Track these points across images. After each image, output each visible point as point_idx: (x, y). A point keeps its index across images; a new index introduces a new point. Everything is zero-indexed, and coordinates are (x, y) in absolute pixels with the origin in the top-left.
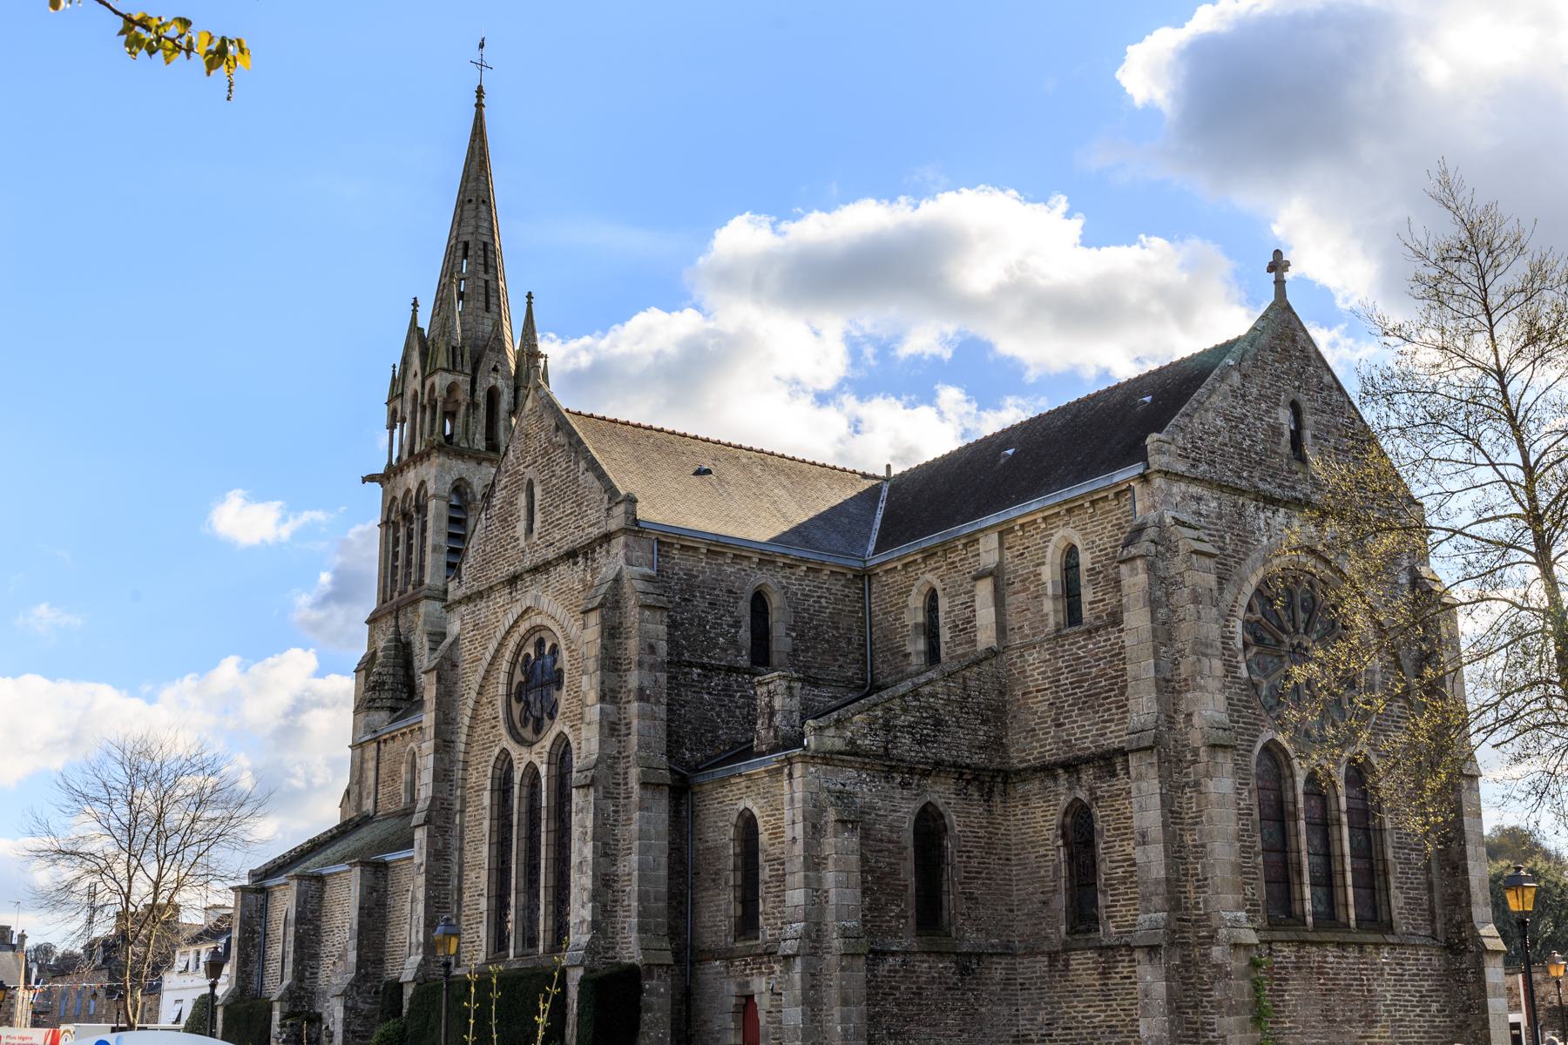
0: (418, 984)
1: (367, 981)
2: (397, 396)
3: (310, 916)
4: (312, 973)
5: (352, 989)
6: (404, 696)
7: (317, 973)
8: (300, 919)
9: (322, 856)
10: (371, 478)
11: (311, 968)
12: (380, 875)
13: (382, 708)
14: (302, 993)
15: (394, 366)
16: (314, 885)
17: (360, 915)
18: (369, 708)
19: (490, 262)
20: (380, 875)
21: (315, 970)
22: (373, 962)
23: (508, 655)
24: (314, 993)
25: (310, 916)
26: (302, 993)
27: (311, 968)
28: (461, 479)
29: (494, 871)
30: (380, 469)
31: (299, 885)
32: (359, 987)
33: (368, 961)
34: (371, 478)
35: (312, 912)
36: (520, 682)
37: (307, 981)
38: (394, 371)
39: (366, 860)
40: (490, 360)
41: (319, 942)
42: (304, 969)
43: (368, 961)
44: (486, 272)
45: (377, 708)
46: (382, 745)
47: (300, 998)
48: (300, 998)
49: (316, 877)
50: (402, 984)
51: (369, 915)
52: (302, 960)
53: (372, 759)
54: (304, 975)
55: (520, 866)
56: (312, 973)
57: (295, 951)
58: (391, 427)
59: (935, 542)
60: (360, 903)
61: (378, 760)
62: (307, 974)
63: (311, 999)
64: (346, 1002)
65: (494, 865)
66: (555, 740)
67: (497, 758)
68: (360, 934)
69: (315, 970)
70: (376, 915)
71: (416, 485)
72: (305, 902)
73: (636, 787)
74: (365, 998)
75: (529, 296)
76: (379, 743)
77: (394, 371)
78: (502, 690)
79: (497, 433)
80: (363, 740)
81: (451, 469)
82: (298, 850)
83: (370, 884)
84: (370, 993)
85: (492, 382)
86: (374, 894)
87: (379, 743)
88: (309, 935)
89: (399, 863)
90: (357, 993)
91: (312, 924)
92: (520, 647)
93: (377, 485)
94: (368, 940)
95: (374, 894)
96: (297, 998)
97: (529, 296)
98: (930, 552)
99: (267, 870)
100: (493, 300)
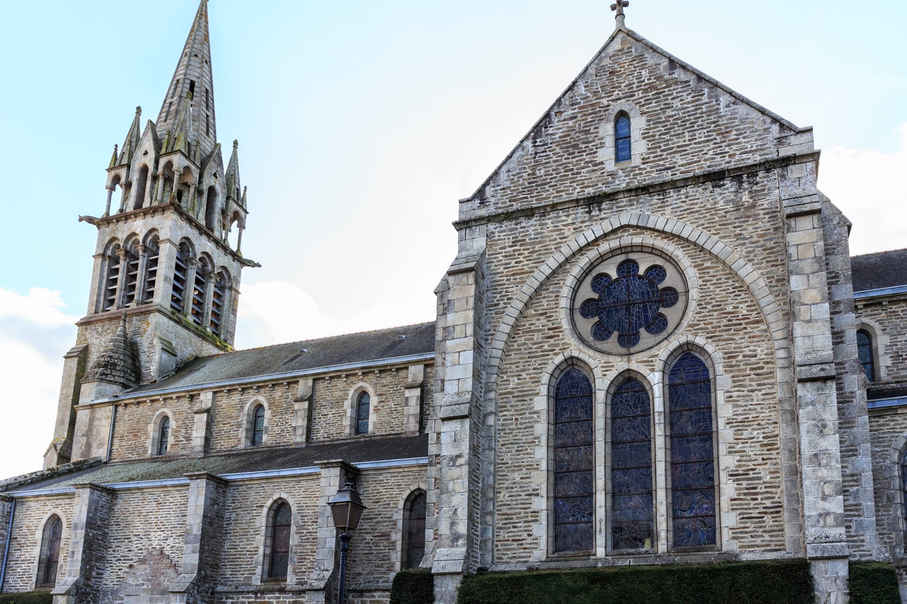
0: (465, 576)
1: (206, 582)
2: (121, 166)
3: (99, 523)
4: (98, 574)
5: (193, 588)
6: (133, 379)
7: (102, 574)
8: (90, 524)
9: (48, 488)
10: (90, 220)
11: (98, 568)
12: (221, 491)
13: (115, 382)
14: (88, 590)
15: (116, 146)
16: (105, 498)
17: (204, 523)
18: (102, 380)
19: (210, 104)
20: (221, 491)
21: (102, 571)
22: (211, 567)
23: (584, 261)
24: (99, 591)
25: (99, 523)
26: (88, 590)
27: (98, 568)
28: (187, 239)
29: (552, 473)
30: (99, 214)
31: (92, 493)
32: (199, 586)
33: (208, 564)
34: (90, 220)
35: (101, 520)
36: (590, 300)
37: (93, 580)
38: (116, 150)
39: (213, 474)
40: (211, 167)
41: (107, 548)
42: (91, 569)
43: (208, 564)
44: (207, 109)
45: (110, 382)
46: (120, 409)
47: (86, 594)
48: (86, 594)
49: (109, 490)
50: (52, 595)
51: (211, 524)
52: (91, 560)
53: (107, 418)
54: (91, 574)
55: (607, 469)
56: (98, 574)
57: (84, 552)
58: (112, 189)
59: (885, 293)
60: (204, 512)
61: (114, 419)
62: (94, 574)
63: (96, 596)
64: (188, 599)
65: (551, 468)
66: (675, 350)
67: (558, 367)
68: (202, 539)
69: (102, 571)
70: (216, 526)
71: (145, 231)
72: (96, 509)
73: (859, 393)
74: (203, 597)
75: (236, 143)
76: (116, 406)
77: (116, 150)
78: (564, 303)
79: (213, 224)
80: (96, 402)
81: (181, 228)
82: (39, 474)
83: (213, 496)
84: (207, 593)
85: (213, 183)
86: (215, 506)
87: (116, 406)
88: (98, 539)
89: (247, 483)
90: (198, 591)
91: (101, 530)
92: (602, 258)
93: (94, 227)
94: (208, 545)
95: (215, 506)
96: (83, 593)
97: (236, 143)
98: (876, 301)
99: (8, 484)
100: (211, 131)
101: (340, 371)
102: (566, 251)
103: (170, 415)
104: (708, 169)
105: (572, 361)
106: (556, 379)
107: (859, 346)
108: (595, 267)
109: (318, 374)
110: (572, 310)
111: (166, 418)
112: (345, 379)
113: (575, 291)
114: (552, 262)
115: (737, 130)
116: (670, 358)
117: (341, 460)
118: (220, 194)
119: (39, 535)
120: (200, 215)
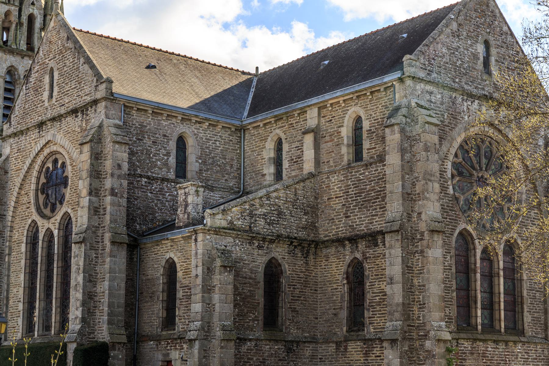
28: (12, 66)
67: (30, 225)
92: (44, 163)
101: (337, 97)
102: (32, 156)
103: (283, 136)
104: (74, 106)
105: (33, 221)
106: (32, 232)
107: (362, 144)
108: (45, 163)
109: (374, 86)
110: (37, 190)
111: (358, 120)
112: (384, 93)
113: (38, 178)
114: (28, 162)
115: (84, 81)
116: (62, 221)
117: (180, 236)
118: (39, 16)
119: (21, 306)
120: (22, 42)
